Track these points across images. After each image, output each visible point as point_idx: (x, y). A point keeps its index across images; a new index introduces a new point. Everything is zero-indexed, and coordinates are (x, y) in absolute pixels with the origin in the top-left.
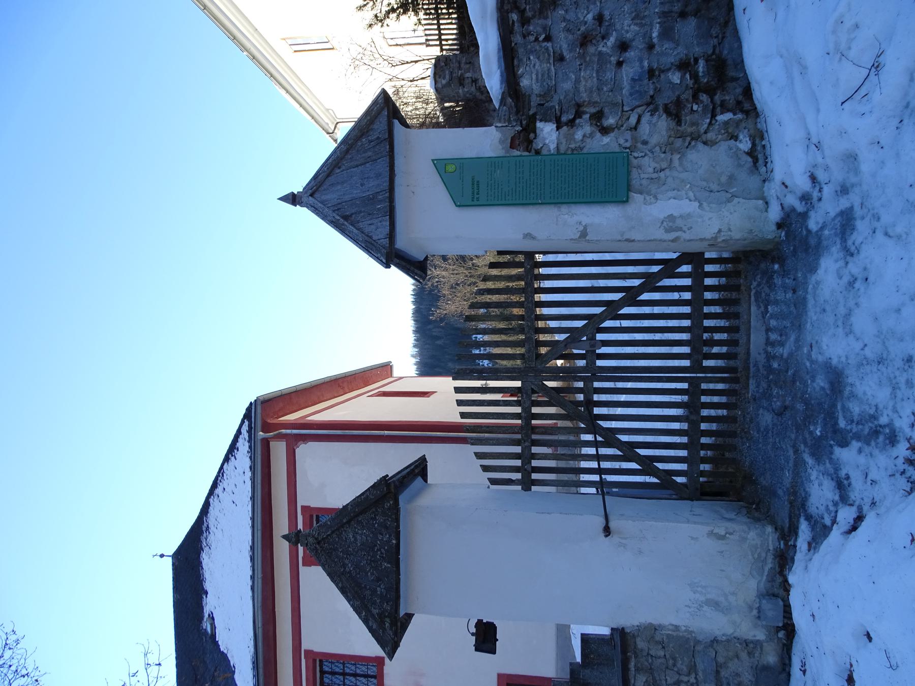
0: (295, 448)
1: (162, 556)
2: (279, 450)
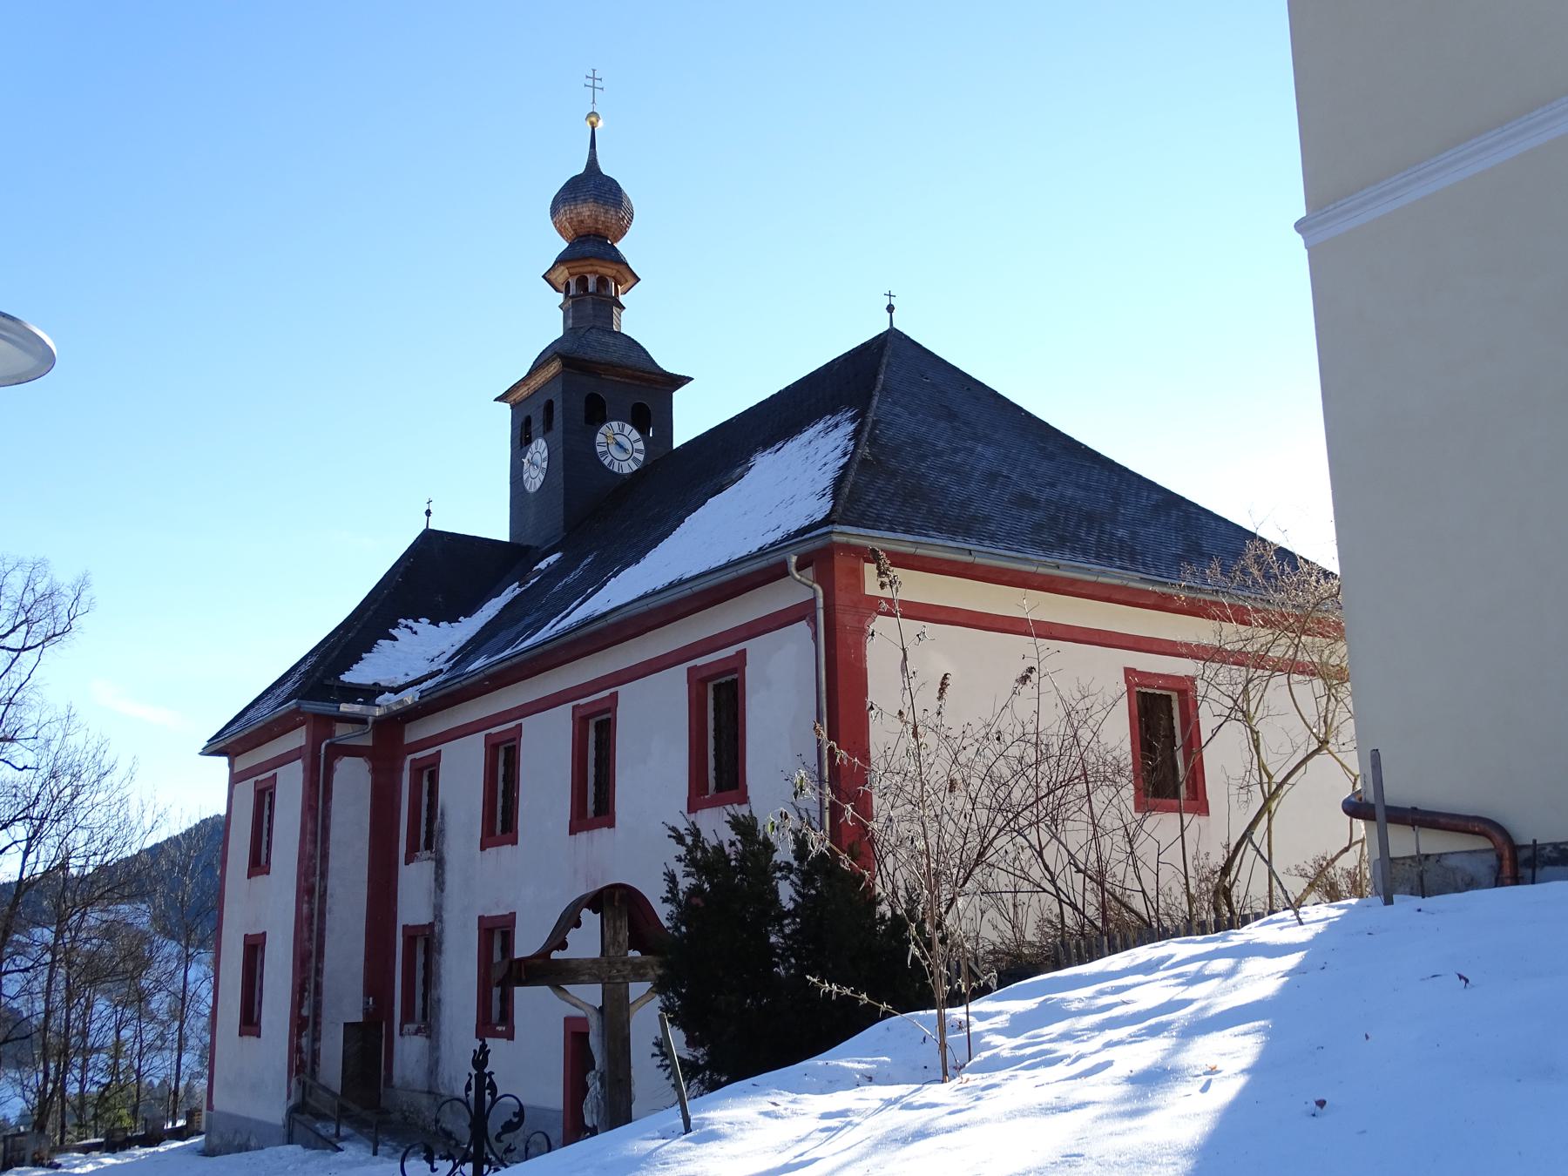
0: (808, 618)
1: (890, 309)
2: (797, 589)
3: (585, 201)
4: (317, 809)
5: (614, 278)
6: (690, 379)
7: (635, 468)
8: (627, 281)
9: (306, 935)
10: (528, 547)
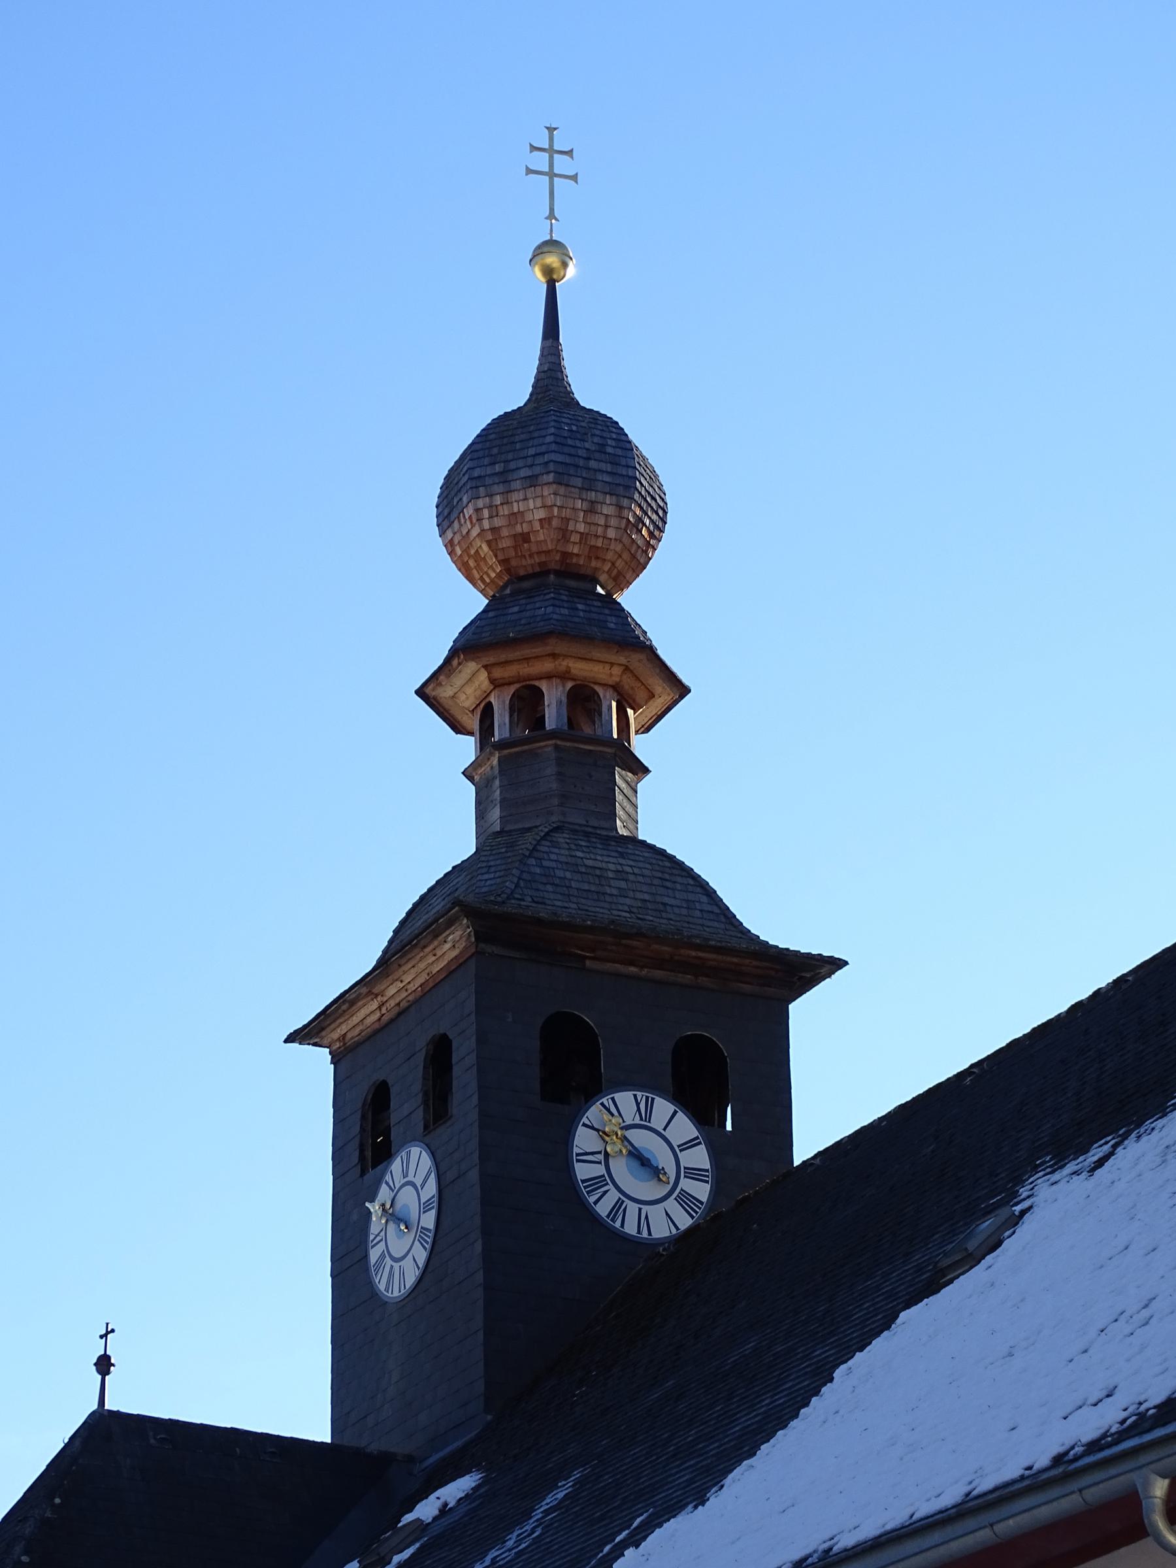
3: (532, 481)
5: (616, 688)
6: (836, 964)
7: (685, 1222)
8: (652, 696)
10: (386, 1459)
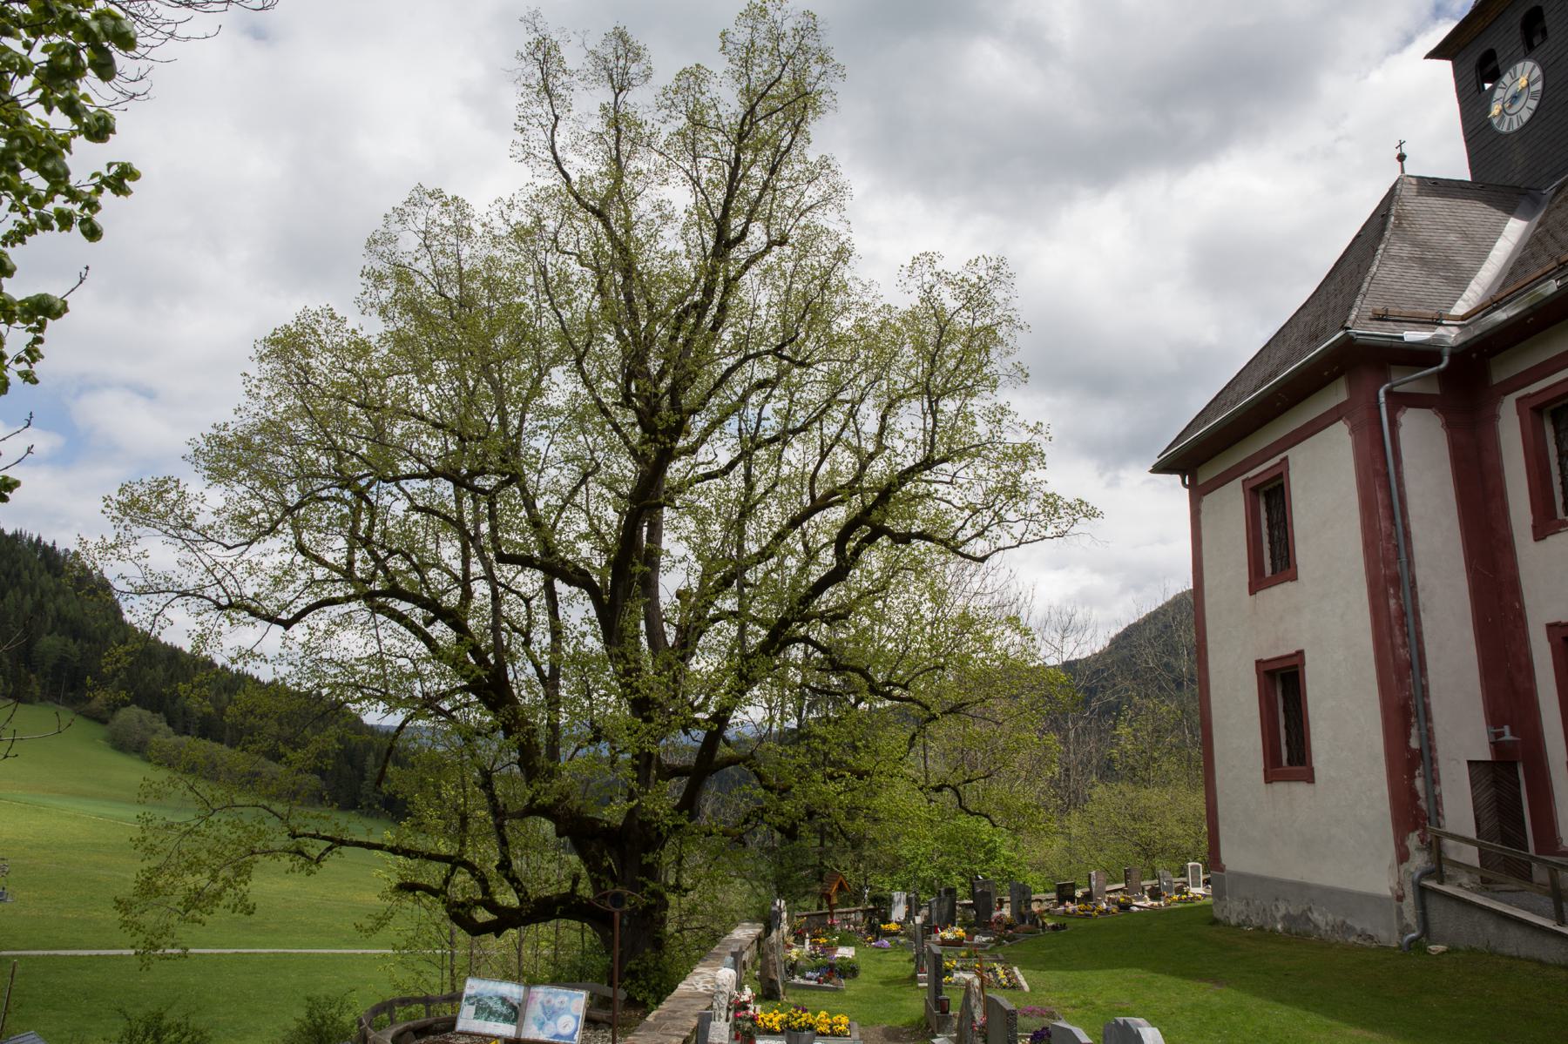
4: (1387, 474)
9: (1399, 641)
